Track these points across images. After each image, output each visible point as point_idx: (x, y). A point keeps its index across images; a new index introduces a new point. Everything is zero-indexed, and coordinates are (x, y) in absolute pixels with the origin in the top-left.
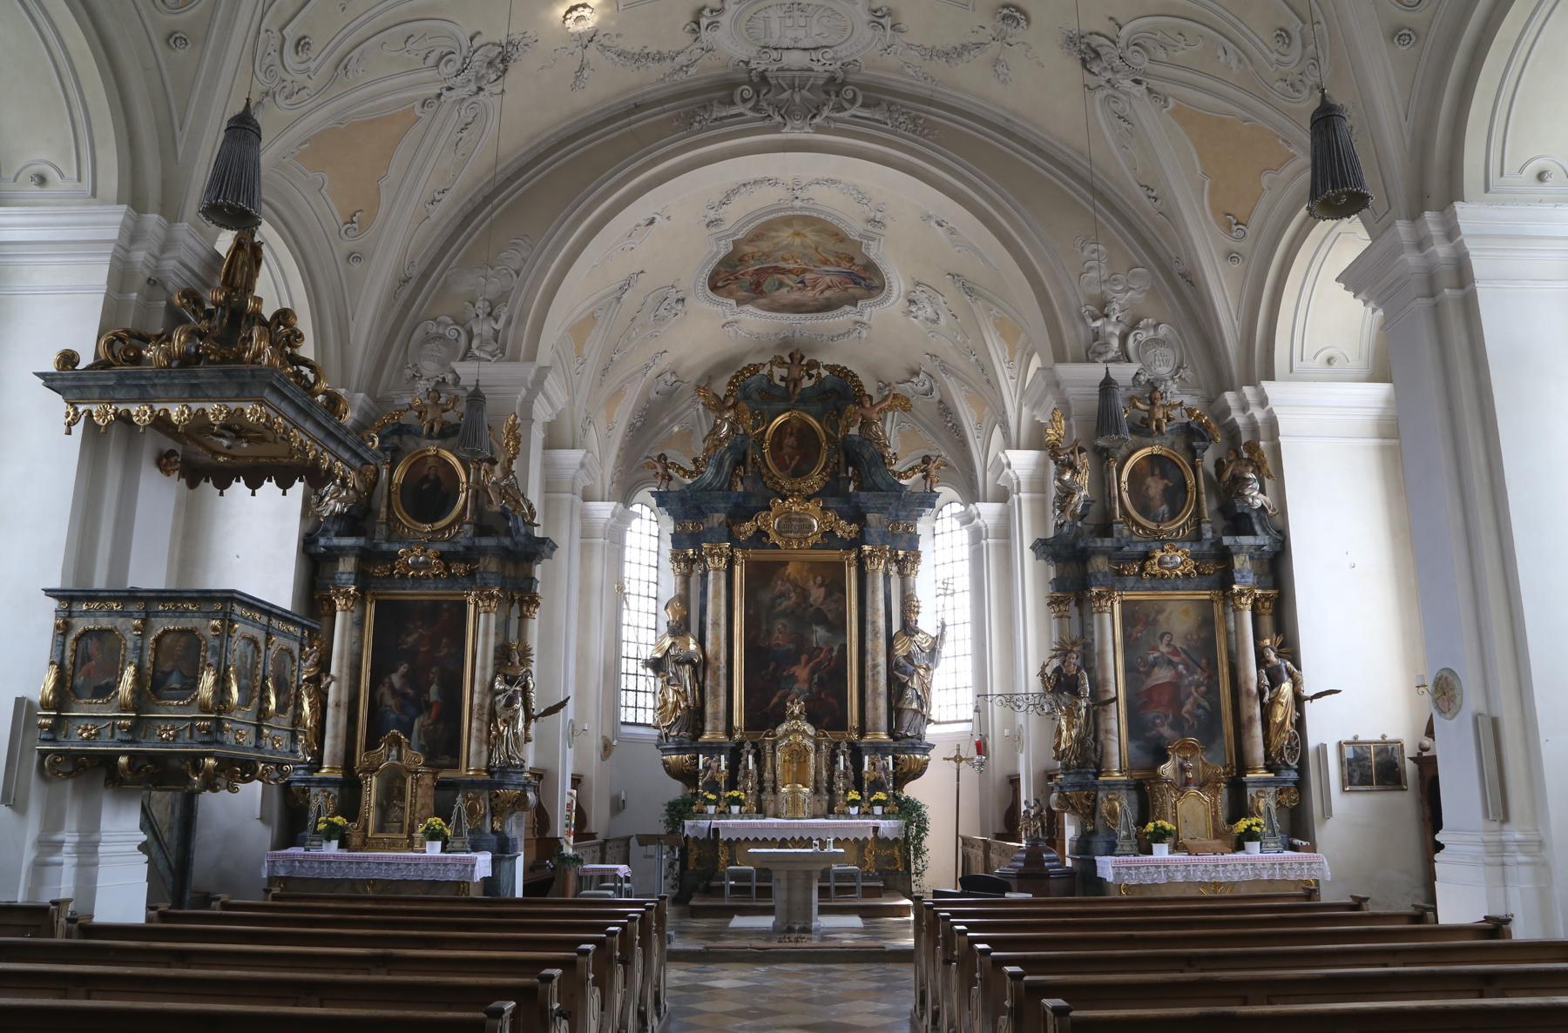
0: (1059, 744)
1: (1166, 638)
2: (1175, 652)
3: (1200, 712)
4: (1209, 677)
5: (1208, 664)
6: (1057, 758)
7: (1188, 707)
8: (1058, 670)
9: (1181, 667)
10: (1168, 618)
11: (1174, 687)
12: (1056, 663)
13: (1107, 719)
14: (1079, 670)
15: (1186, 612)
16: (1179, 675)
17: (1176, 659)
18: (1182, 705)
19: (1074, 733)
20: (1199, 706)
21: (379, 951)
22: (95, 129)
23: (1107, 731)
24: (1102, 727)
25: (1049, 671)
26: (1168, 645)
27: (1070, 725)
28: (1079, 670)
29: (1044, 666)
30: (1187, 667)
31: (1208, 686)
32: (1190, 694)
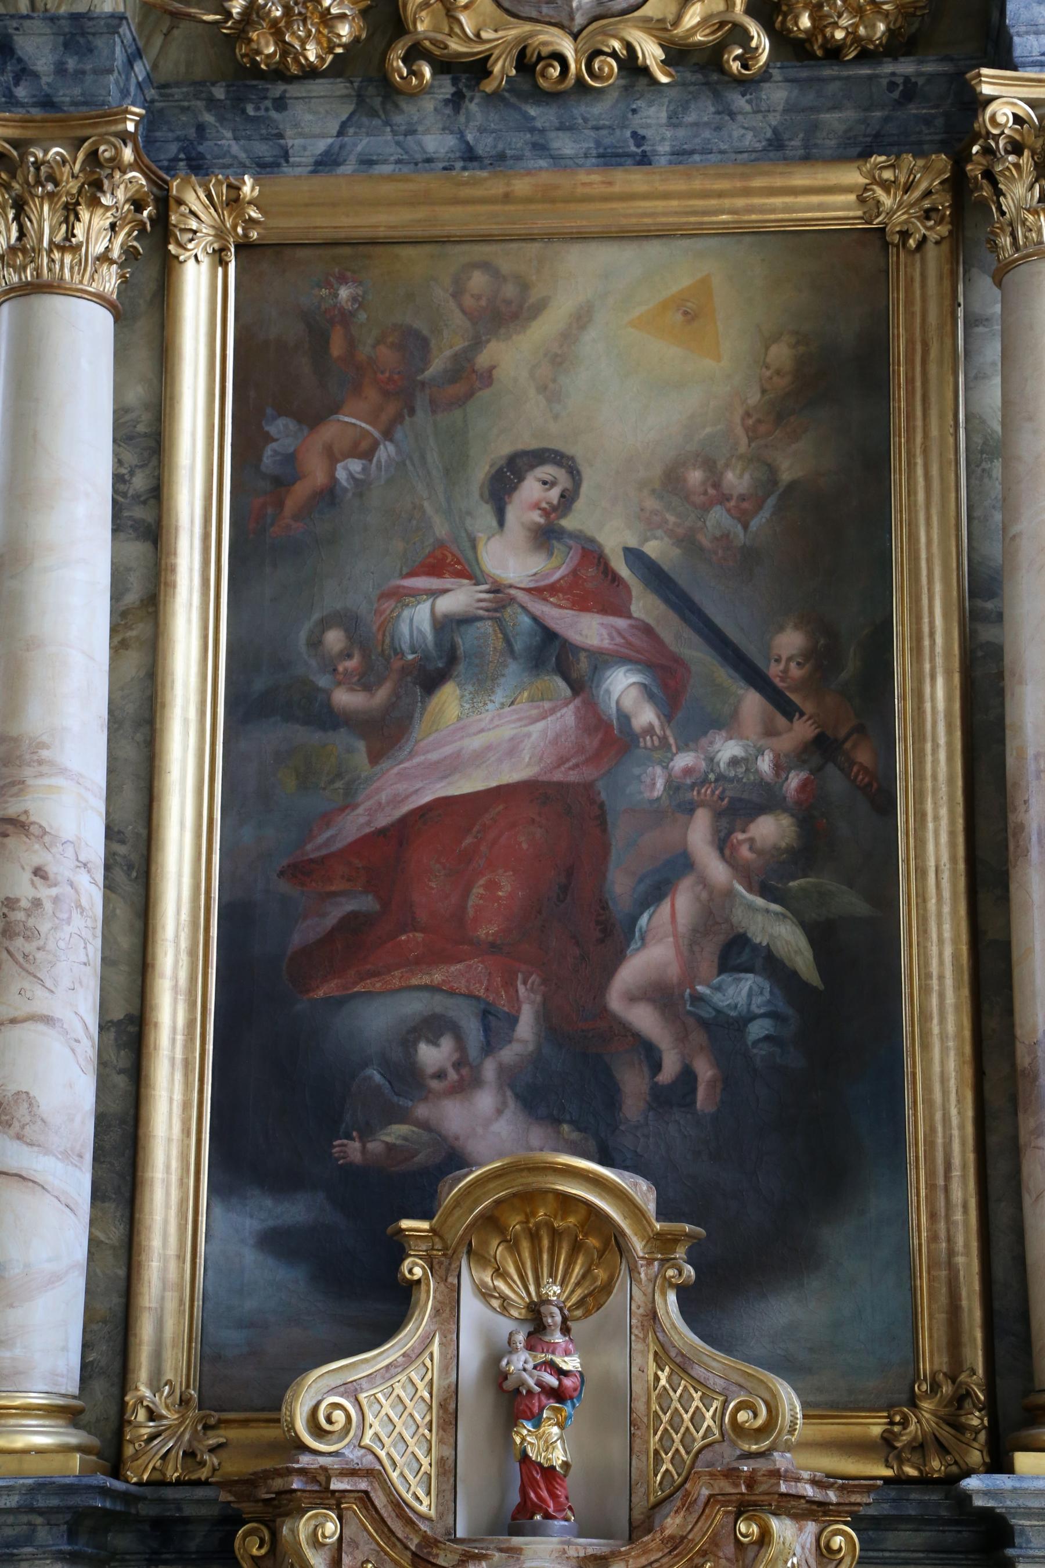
1: (533, 491)
2: (593, 582)
3: (742, 992)
4: (823, 748)
5: (822, 659)
7: (654, 954)
9: (622, 686)
10: (559, 358)
11: (566, 820)
15: (690, 313)
16: (611, 740)
17: (590, 630)
18: (613, 937)
20: (736, 953)
26: (546, 536)
30: (667, 682)
31: (810, 816)
32: (682, 863)
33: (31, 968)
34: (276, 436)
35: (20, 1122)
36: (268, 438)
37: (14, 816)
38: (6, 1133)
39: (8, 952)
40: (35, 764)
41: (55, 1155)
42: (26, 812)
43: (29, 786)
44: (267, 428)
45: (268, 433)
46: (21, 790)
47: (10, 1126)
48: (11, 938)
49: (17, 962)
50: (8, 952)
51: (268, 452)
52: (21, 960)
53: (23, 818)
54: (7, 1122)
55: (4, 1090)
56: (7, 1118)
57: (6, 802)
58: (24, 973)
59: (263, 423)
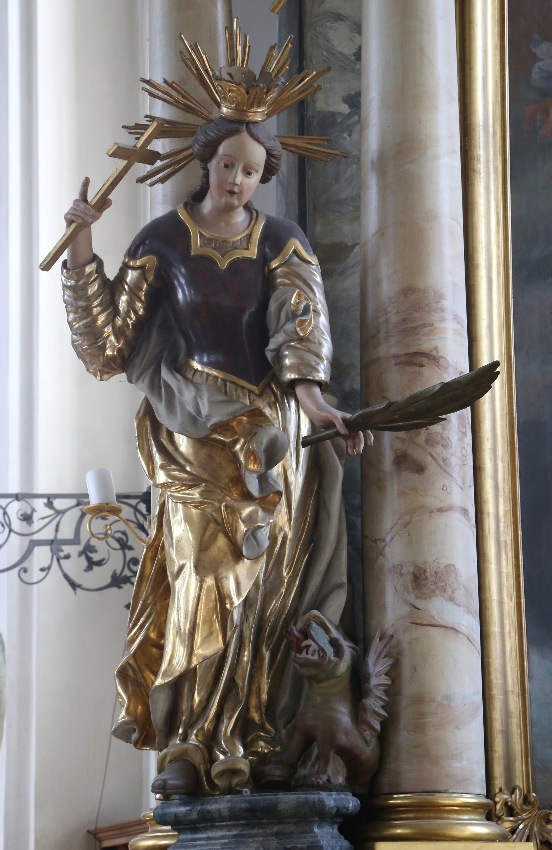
0: (151, 651)
6: (142, 731)
8: (161, 240)
12: (156, 201)
13: (418, 516)
14: (274, 239)
19: (241, 580)
21: (398, 424)
22: (478, 845)
23: (422, 580)
24: (394, 552)
25: (111, 242)
27: (219, 543)
28: (274, 239)
29: (84, 214)
33: (445, 467)
34: (541, 57)
35: (451, 587)
36: (536, 59)
37: (427, 351)
38: (443, 596)
39: (432, 456)
40: (439, 311)
41: (472, 614)
42: (436, 348)
43: (436, 328)
44: (534, 50)
45: (535, 54)
46: (431, 331)
47: (445, 590)
48: (433, 446)
49: (439, 464)
50: (432, 456)
51: (535, 70)
52: (442, 463)
53: (434, 353)
54: (442, 587)
55: (438, 563)
56: (442, 584)
57: (420, 340)
58: (444, 473)
59: (531, 46)
